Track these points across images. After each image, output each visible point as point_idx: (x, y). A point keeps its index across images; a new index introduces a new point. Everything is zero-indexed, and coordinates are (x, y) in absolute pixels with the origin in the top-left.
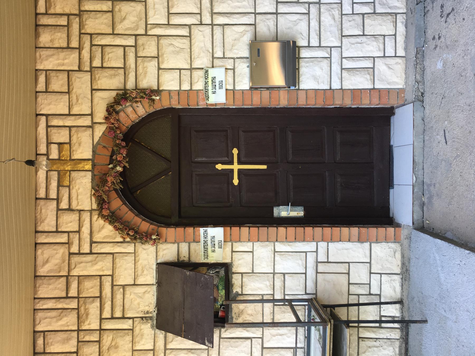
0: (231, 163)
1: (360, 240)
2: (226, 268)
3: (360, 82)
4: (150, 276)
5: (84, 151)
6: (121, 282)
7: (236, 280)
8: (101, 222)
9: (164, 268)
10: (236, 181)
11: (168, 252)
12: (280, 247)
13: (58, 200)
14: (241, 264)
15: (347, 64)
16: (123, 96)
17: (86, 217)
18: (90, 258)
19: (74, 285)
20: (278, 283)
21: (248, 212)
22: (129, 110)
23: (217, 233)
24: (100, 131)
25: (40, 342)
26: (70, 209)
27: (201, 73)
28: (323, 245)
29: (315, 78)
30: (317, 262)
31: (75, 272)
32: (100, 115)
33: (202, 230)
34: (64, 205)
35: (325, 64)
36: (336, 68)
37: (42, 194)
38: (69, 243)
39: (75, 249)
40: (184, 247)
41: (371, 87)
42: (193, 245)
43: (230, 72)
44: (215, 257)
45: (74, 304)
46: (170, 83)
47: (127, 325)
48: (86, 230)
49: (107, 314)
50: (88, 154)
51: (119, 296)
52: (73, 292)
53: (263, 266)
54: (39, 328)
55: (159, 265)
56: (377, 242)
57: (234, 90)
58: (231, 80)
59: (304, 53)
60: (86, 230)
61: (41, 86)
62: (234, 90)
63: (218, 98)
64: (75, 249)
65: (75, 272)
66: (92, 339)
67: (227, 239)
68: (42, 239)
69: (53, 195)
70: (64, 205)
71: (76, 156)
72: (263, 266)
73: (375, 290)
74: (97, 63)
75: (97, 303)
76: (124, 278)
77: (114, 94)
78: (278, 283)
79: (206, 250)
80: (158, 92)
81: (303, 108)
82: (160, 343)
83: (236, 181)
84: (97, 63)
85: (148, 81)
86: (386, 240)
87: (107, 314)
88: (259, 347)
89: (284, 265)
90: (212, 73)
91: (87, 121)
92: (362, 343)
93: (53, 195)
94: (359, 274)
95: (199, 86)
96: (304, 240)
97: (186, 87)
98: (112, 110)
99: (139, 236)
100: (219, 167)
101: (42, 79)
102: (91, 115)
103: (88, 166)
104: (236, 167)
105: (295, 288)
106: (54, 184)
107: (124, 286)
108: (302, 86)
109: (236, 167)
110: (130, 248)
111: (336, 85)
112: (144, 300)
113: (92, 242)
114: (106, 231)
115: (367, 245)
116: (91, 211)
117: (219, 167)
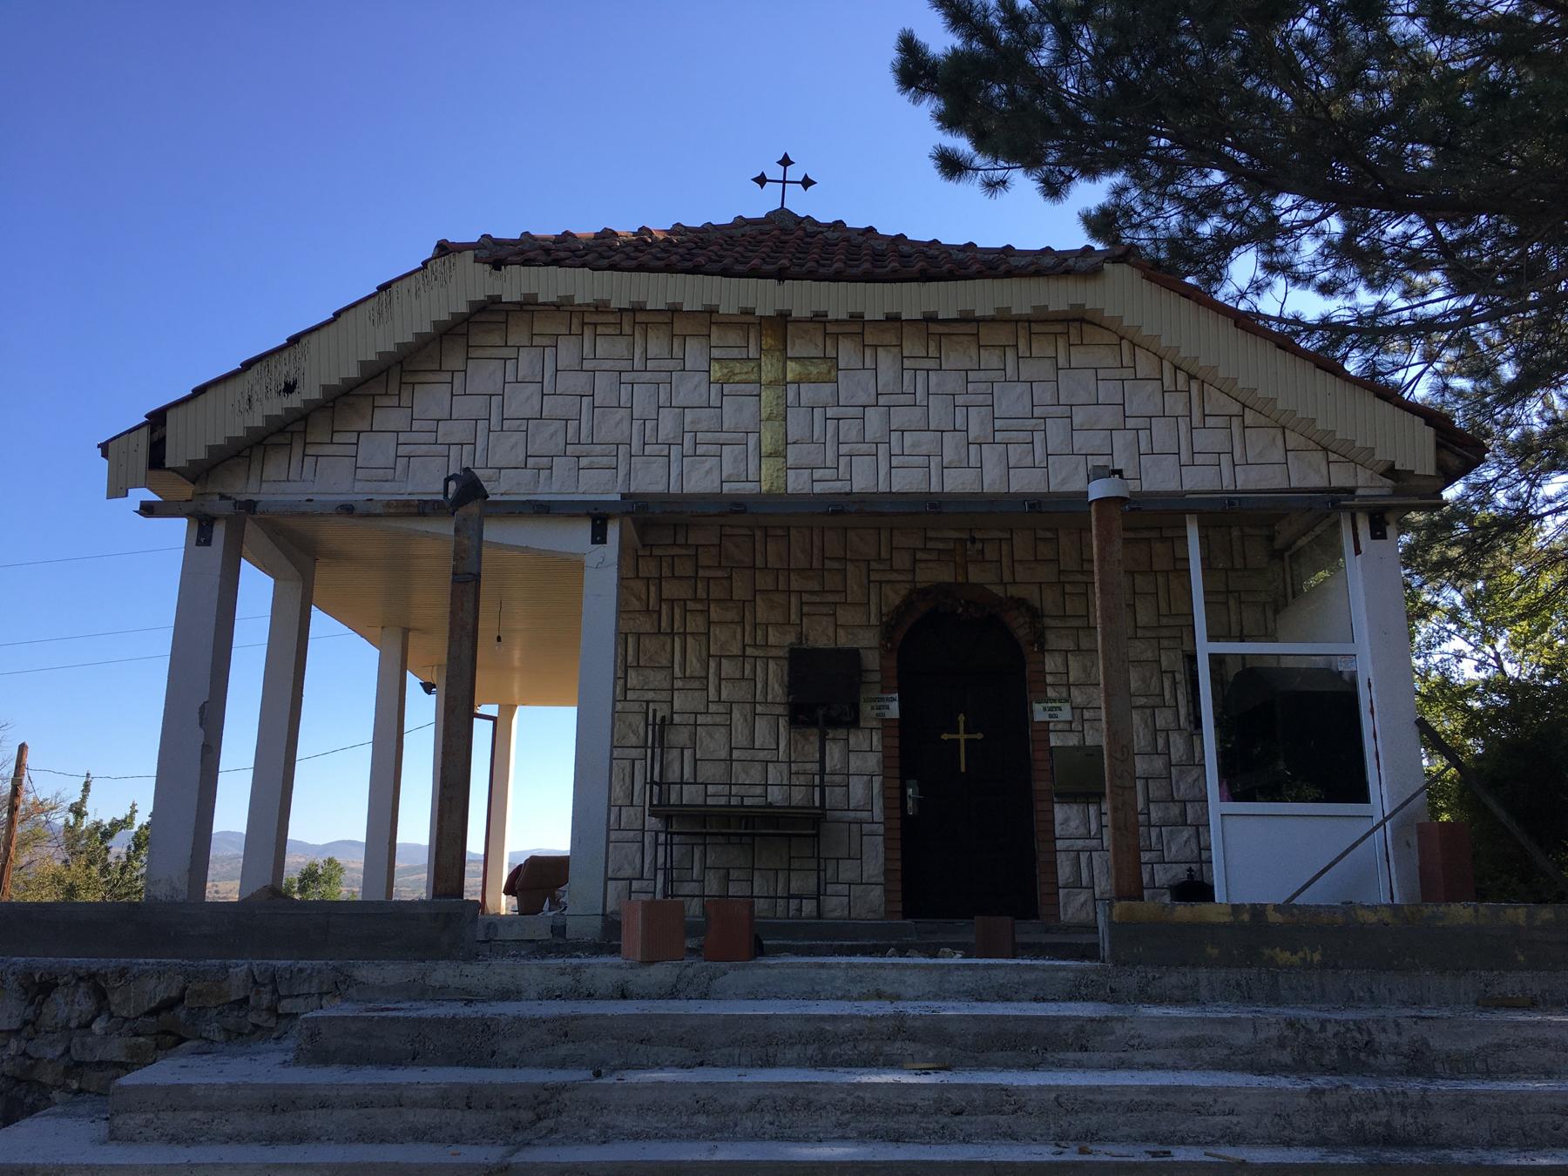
0: (967, 731)
1: (887, 872)
2: (854, 723)
3: (1064, 871)
4: (844, 641)
5: (975, 575)
6: (840, 612)
7: (841, 733)
8: (904, 592)
9: (854, 655)
10: (945, 737)
11: (872, 660)
12: (877, 781)
13: (924, 549)
14: (857, 739)
15: (1084, 858)
16: (1036, 614)
17: (910, 577)
18: (704, 654)
19: (836, 565)
20: (837, 779)
21: (912, 752)
22: (1021, 620)
23: (894, 711)
24: (998, 590)
25: (780, 532)
26: (915, 561)
27: (1065, 695)
28: (881, 829)
29: (1066, 821)
30: (861, 823)
31: (850, 566)
32: (1013, 591)
33: (896, 695)
34: (919, 555)
35: (1082, 831)
36: (1080, 844)
37: (931, 534)
38: (879, 560)
39: (874, 565)
40: (877, 677)
41: (1060, 883)
42: (878, 687)
43: (1067, 727)
44: (867, 709)
45: (816, 565)
46: (1051, 663)
47: (794, 617)
48: (895, 577)
49: (805, 598)
50: (973, 579)
51: (825, 610)
52: (828, 564)
53: (855, 763)
54: (793, 532)
55: (856, 651)
56: (886, 891)
57: (1049, 731)
58: (1060, 727)
59: (1092, 809)
60: (895, 577)
61: (1041, 534)
62: (1049, 731)
63: (1039, 713)
64: (874, 565)
65: (850, 566)
66: (663, 625)
67: (886, 722)
68: (884, 536)
69: (930, 545)
70: (919, 555)
71: (971, 568)
72: (855, 763)
73: (830, 889)
74: (1068, 588)
75: (817, 588)
76: (844, 616)
77: (1038, 605)
78: (837, 779)
79: (874, 700)
80: (1042, 650)
81: (942, 1163)
82: (774, 652)
83: (945, 737)
84: (1068, 588)
85: (1053, 640)
86: (888, 902)
87: (805, 598)
88: (769, 758)
89: (857, 788)
90: (1066, 707)
91: (1007, 578)
92: (772, 873)
93: (930, 545)
94: (848, 871)
95: (1051, 693)
96: (885, 808)
97: (1049, 679)
98: (1020, 602)
99: (888, 630)
100: (962, 718)
101: (1049, 535)
102: (1014, 582)
103: (960, 579)
104: (962, 737)
105: (834, 796)
106: (941, 546)
107: (834, 614)
108: (1057, 807)
109: (962, 737)
110: (874, 621)
111: (1060, 844)
112: (821, 636)
113: (881, 583)
114: (894, 598)
115: (882, 879)
116: (914, 581)
117: (962, 718)
